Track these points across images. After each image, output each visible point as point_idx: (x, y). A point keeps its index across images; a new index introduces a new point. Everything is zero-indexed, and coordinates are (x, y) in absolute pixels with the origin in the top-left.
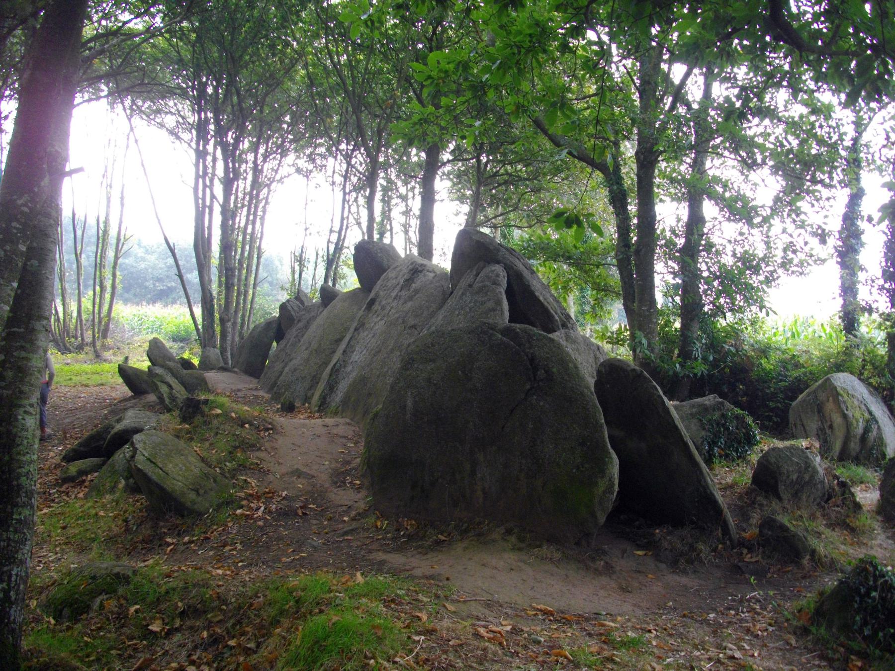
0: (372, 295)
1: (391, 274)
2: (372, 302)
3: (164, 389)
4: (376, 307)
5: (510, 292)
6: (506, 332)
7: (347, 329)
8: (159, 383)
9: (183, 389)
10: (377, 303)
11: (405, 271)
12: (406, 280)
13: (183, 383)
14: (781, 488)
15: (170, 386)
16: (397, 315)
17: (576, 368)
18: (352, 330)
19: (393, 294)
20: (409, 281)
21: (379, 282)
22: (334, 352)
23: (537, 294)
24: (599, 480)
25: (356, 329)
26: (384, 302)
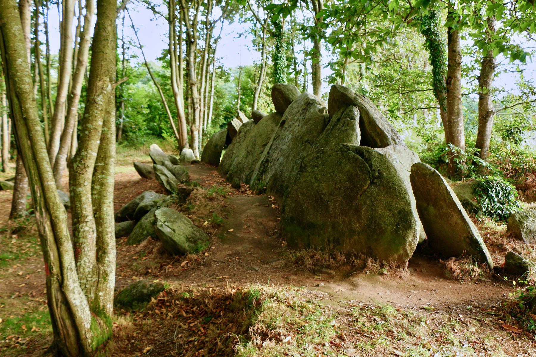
0: (283, 118)
1: (294, 105)
2: (284, 122)
3: (163, 178)
4: (286, 126)
5: (361, 123)
6: (357, 150)
7: (269, 138)
8: (160, 175)
9: (174, 177)
10: (286, 123)
11: (303, 103)
12: (303, 109)
13: (174, 174)
14: (523, 234)
15: (166, 175)
16: (298, 134)
17: (396, 171)
18: (272, 139)
19: (296, 118)
20: (305, 110)
21: (287, 110)
22: (262, 152)
23: (377, 123)
24: (258, 284)
25: (274, 139)
26: (290, 123)
